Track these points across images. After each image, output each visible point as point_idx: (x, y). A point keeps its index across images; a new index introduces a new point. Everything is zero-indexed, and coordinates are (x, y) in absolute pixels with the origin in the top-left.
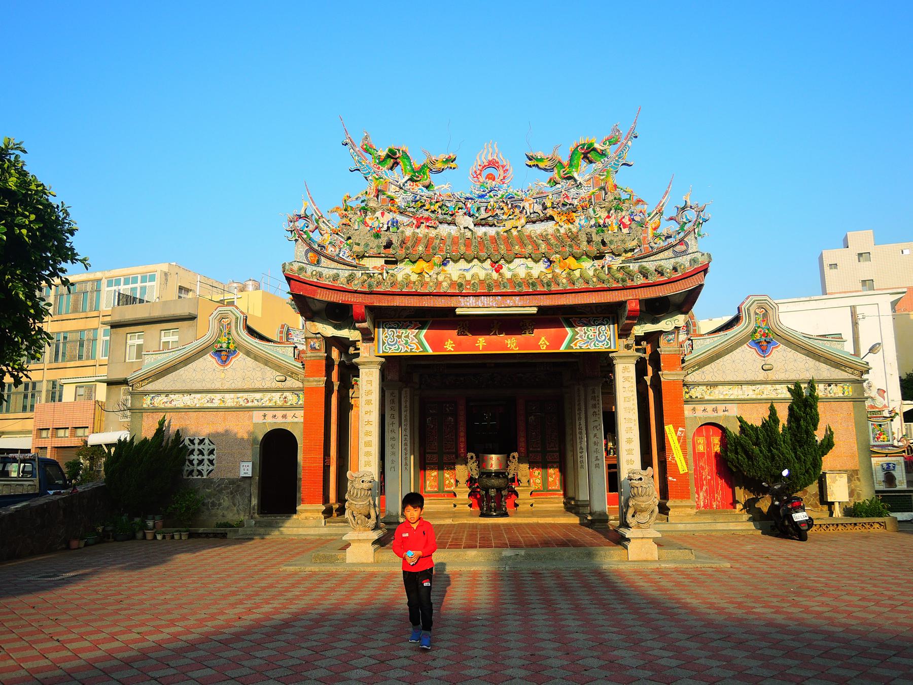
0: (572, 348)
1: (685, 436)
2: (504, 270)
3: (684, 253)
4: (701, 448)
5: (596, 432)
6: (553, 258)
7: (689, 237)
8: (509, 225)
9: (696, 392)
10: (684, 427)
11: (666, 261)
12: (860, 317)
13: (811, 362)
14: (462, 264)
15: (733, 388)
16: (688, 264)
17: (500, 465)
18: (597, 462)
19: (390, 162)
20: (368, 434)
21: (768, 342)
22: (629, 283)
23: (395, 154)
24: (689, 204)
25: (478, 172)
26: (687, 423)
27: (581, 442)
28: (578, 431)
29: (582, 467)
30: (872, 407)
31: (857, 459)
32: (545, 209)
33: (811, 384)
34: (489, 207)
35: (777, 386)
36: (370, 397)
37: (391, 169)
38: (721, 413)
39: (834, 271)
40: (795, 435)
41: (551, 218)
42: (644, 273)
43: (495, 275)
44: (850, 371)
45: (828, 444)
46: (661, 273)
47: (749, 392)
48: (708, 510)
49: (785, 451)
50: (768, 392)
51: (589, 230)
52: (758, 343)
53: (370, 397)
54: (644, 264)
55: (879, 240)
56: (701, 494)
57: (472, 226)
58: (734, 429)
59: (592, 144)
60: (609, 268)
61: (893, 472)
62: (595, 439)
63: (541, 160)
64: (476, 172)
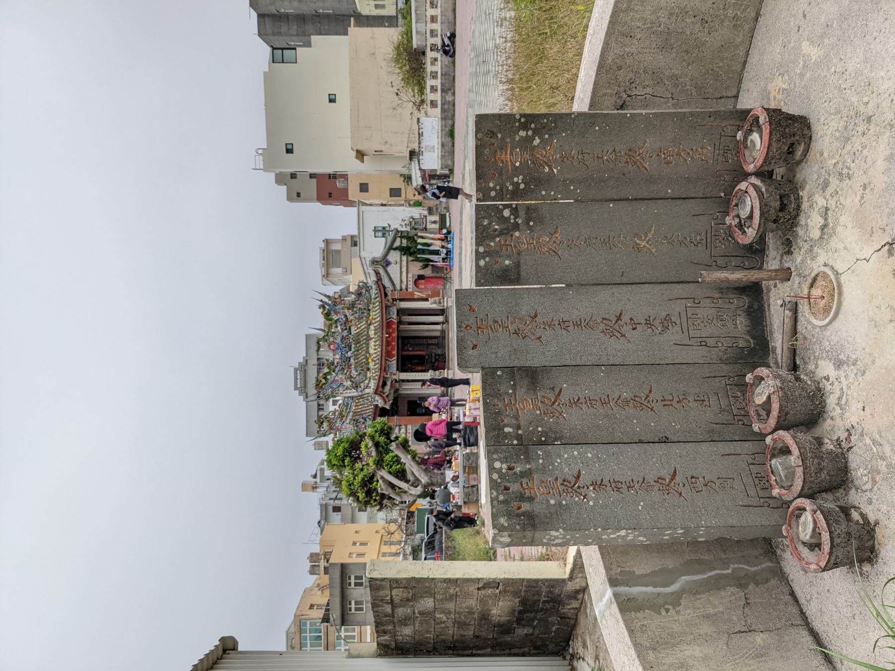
9: (404, 287)
39: (302, 195)
50: (404, 263)
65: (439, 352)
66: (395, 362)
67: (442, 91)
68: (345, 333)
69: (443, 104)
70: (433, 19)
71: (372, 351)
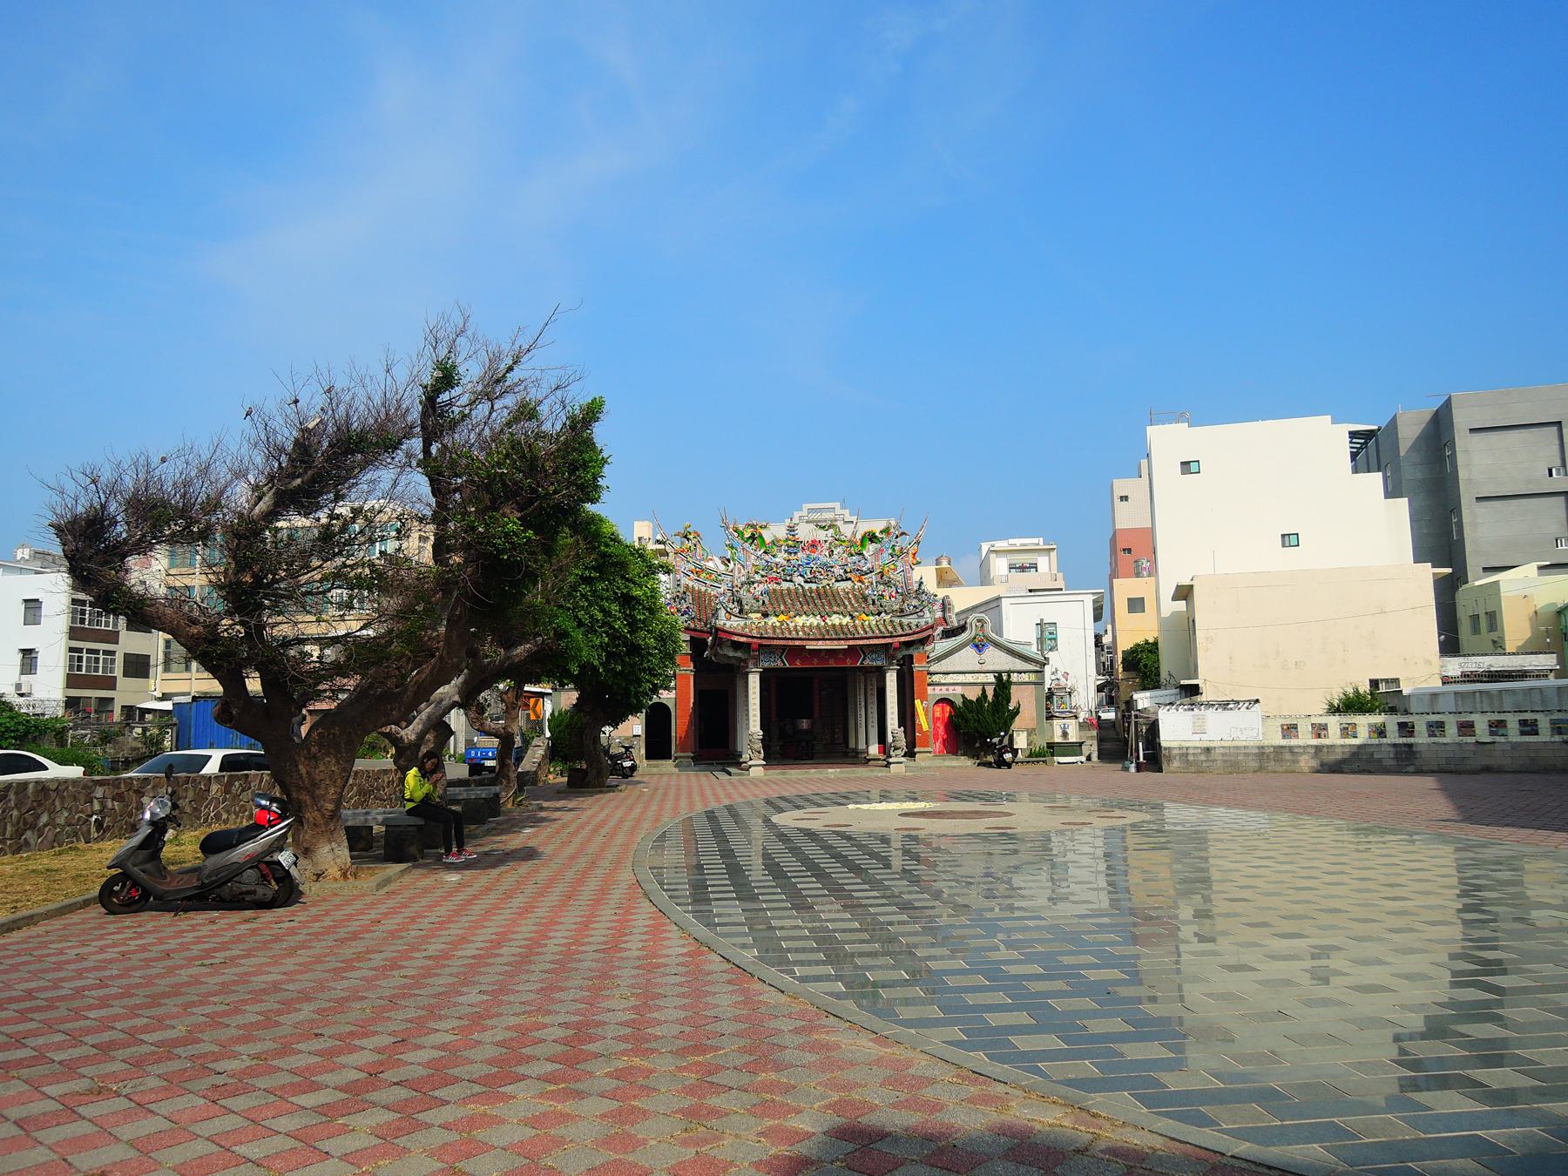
4: (938, 714)
8: (825, 582)
9: (935, 678)
11: (913, 620)
15: (958, 673)
33: (1009, 673)
42: (901, 624)
45: (1016, 712)
47: (970, 678)
50: (982, 678)
58: (959, 702)
66: (779, 664)
67: (1318, 748)
68: (838, 571)
69: (1291, 748)
70: (1466, 728)
71: (800, 621)
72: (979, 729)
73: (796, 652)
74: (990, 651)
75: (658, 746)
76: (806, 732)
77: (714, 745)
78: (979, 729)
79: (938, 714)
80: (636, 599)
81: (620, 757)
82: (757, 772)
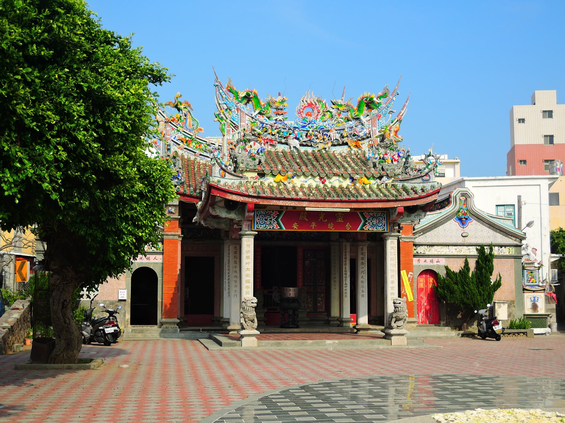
0: (364, 229)
1: (413, 278)
2: (327, 183)
3: (427, 181)
4: (421, 285)
5: (363, 275)
6: (356, 177)
7: (431, 173)
8: (321, 146)
9: (421, 250)
10: (412, 272)
11: (418, 185)
12: (523, 203)
13: (491, 232)
14: (302, 178)
15: (444, 244)
16: (429, 188)
17: (295, 294)
18: (363, 293)
19: (245, 101)
20: (247, 275)
21: (466, 219)
22: (400, 198)
23: (250, 95)
24: (432, 154)
25: (301, 110)
26: (415, 269)
27: (346, 280)
28: (344, 273)
29: (346, 296)
30: (528, 260)
31: (514, 294)
32: (343, 137)
33: (491, 246)
34: (309, 134)
35: (470, 247)
36: (248, 255)
37: (246, 104)
38: (435, 263)
39: (522, 124)
40: (479, 279)
41: (347, 144)
42: (405, 189)
43: (322, 185)
44: (514, 239)
45: (498, 285)
46: (416, 193)
48: (424, 324)
49: (472, 288)
50: (465, 251)
51: (374, 160)
52: (460, 219)
53: (248, 255)
54: (405, 184)
55: (560, 100)
56: (420, 314)
57: (298, 146)
58: (442, 273)
59: (372, 98)
60: (386, 185)
61: (537, 303)
62: (362, 279)
63: (341, 105)
64: (300, 110)
65: (302, 315)
66: (275, 227)
68: (334, 135)
71: (298, 182)
72: (460, 300)
73: (293, 214)
74: (473, 226)
75: (143, 310)
76: (293, 300)
77: (201, 311)
78: (460, 300)
79: (421, 285)
80: (111, 102)
81: (102, 322)
82: (251, 340)
